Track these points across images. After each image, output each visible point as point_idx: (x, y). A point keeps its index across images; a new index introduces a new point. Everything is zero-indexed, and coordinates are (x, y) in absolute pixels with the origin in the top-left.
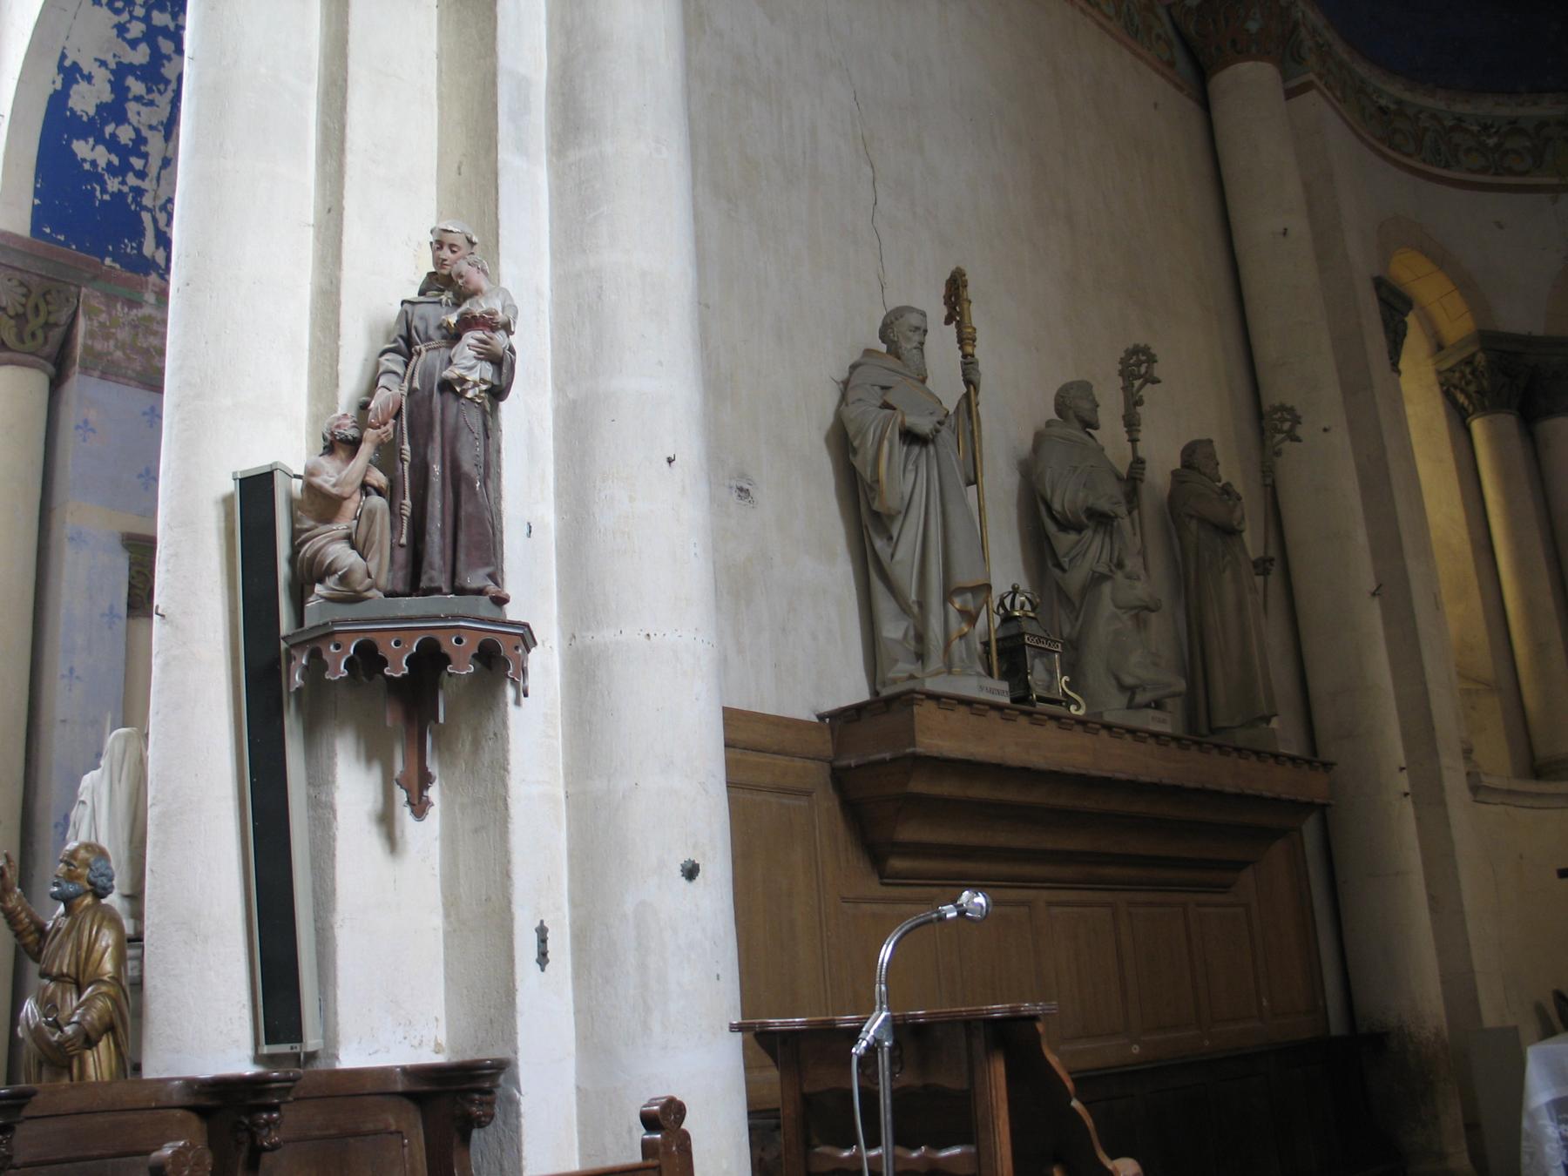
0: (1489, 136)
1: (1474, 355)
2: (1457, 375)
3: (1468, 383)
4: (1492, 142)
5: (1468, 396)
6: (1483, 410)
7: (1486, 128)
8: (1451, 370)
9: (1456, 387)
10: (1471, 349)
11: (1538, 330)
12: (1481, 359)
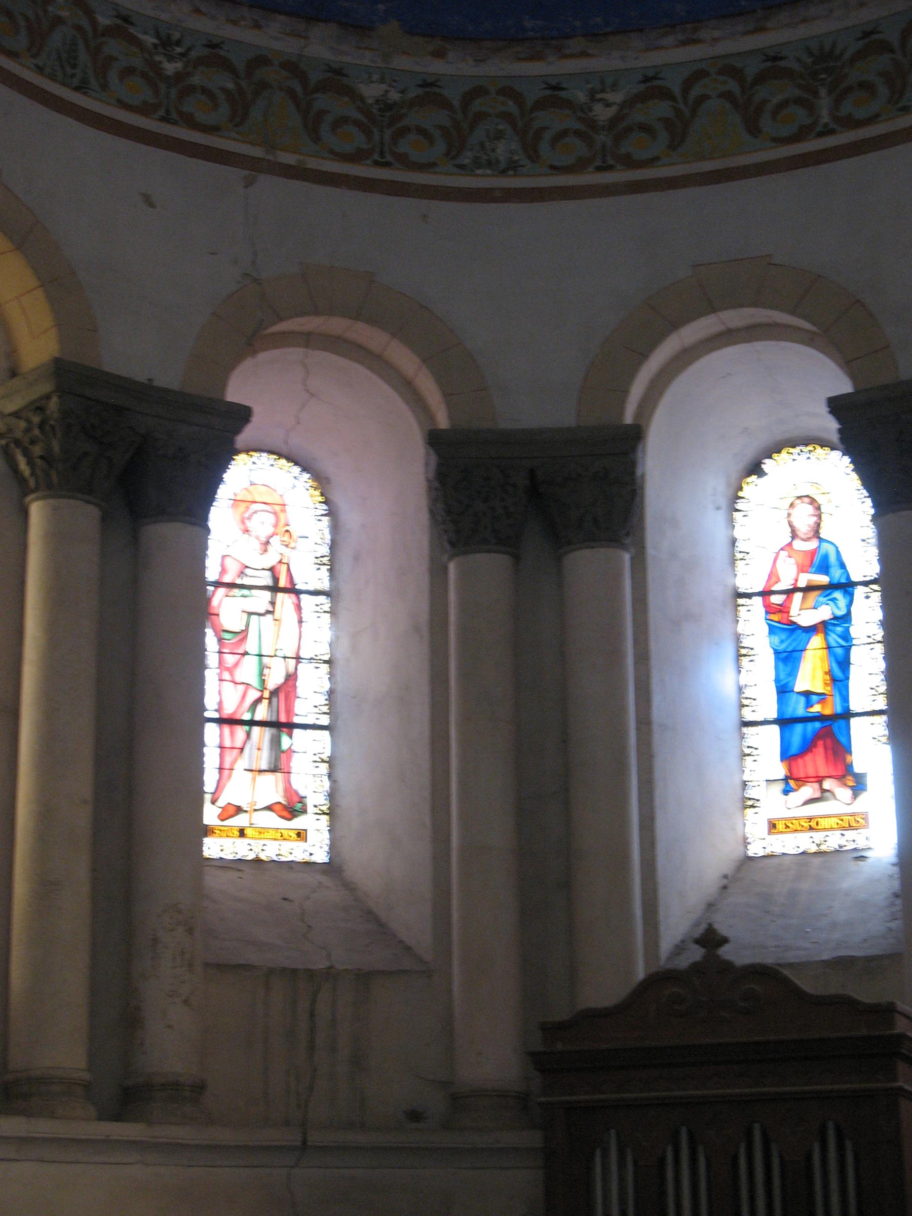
0: (171, 58)
1: (48, 397)
2: (23, 424)
3: (33, 442)
4: (171, 68)
5: (31, 463)
6: (49, 489)
7: (166, 43)
8: (16, 415)
9: (17, 442)
10: (46, 387)
11: (169, 377)
12: (53, 404)
